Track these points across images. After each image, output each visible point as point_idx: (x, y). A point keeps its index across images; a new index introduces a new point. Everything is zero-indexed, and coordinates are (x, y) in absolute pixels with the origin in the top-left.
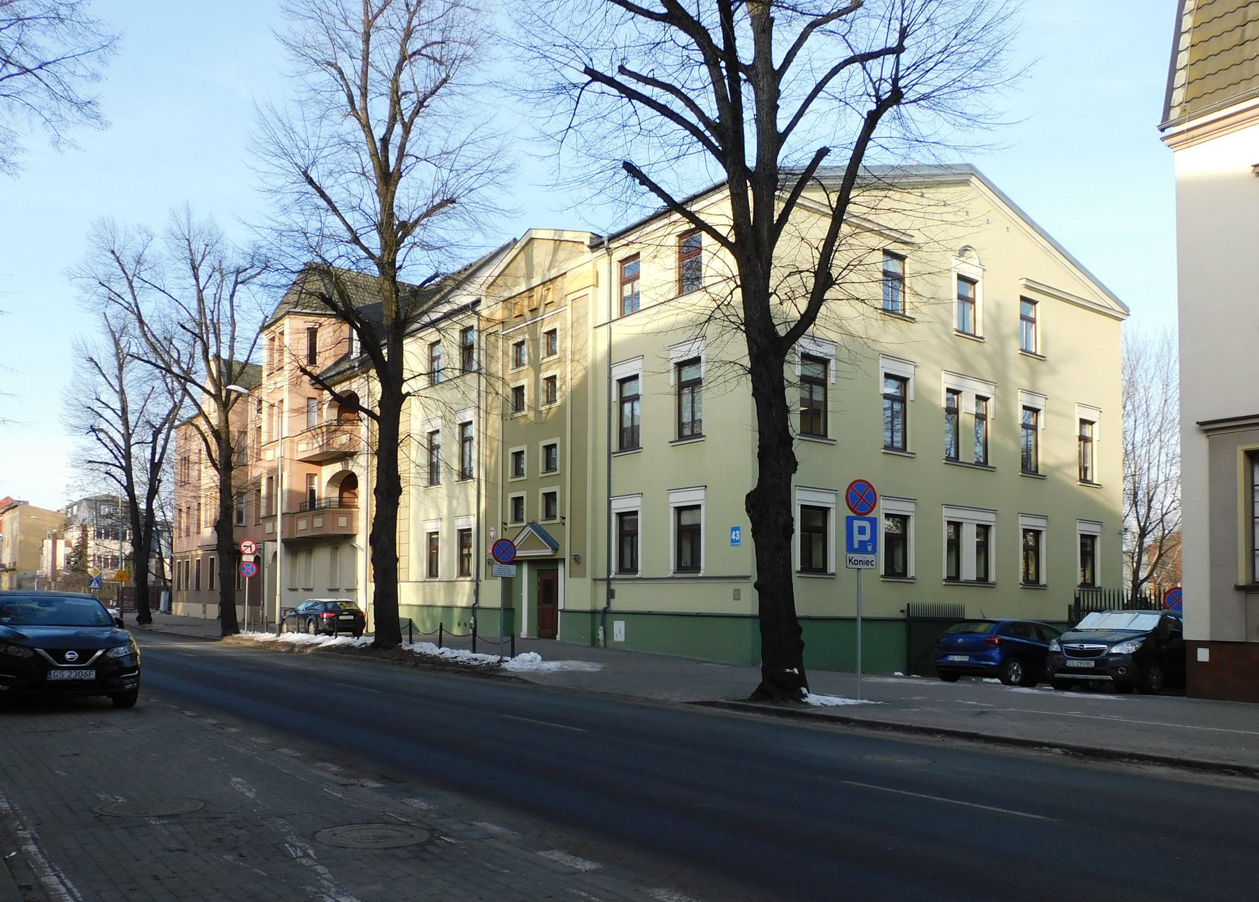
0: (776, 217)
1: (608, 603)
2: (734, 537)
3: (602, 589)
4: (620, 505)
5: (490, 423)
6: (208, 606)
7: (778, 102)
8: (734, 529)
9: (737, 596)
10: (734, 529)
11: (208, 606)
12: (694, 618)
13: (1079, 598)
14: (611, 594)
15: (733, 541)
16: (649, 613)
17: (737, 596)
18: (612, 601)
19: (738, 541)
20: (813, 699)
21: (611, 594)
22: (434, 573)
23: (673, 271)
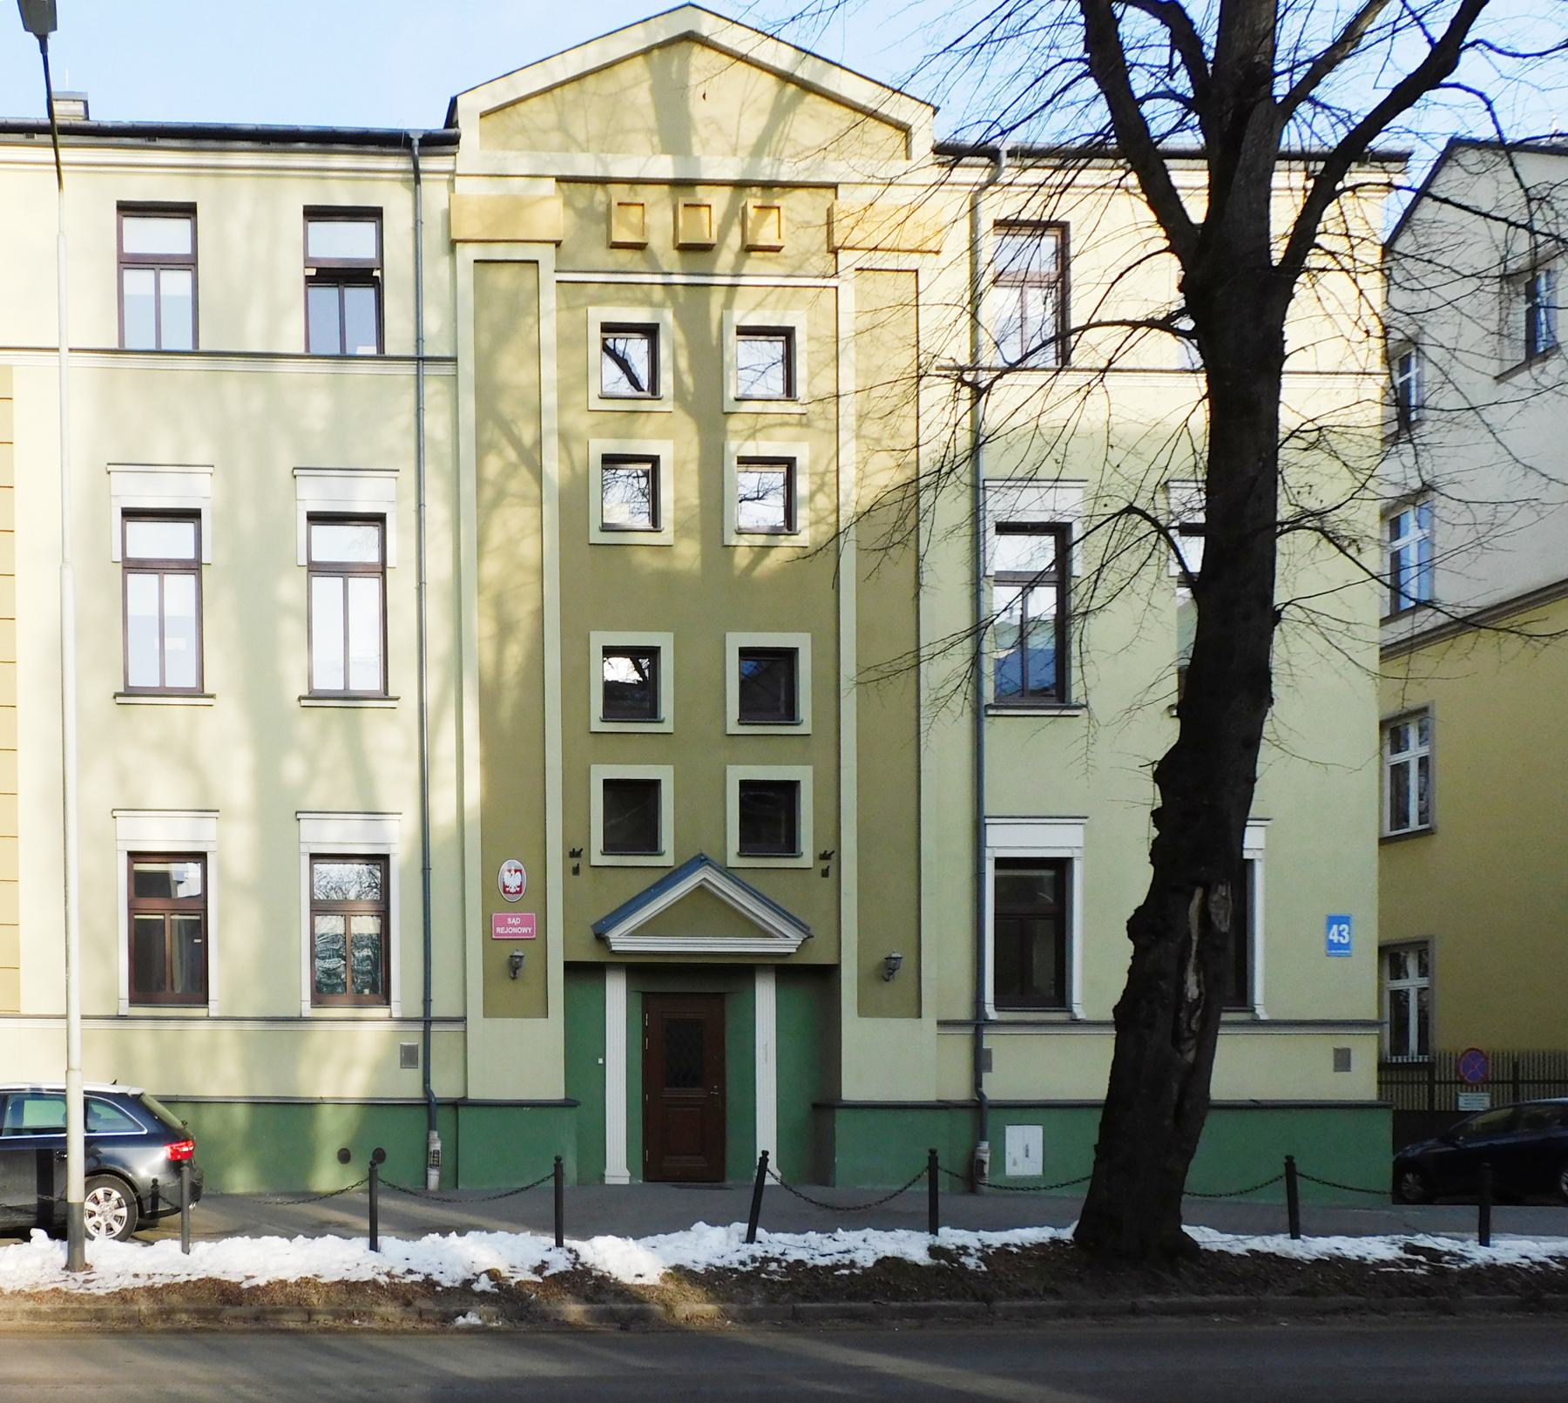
0: (1278, 253)
1: (977, 1083)
2: (1335, 938)
3: (961, 1044)
4: (1005, 840)
5: (496, 537)
6: (1138, 94)
7: (1167, 29)
8: (1334, 920)
9: (1343, 1060)
10: (1334, 920)
11: (1138, 94)
12: (1248, 1113)
13: (1518, 1062)
14: (980, 1062)
15: (1332, 945)
16: (1256, 1106)
17: (1343, 1060)
18: (986, 1077)
19: (1346, 946)
20: (1206, 1237)
21: (980, 1062)
22: (1042, 974)
23: (780, 364)
